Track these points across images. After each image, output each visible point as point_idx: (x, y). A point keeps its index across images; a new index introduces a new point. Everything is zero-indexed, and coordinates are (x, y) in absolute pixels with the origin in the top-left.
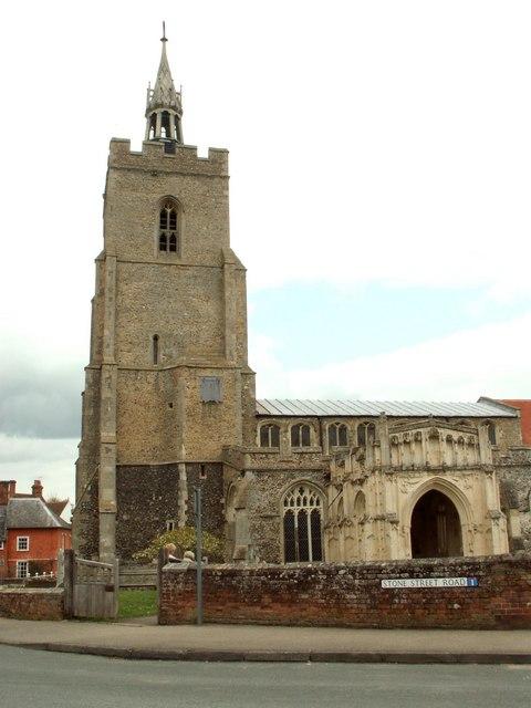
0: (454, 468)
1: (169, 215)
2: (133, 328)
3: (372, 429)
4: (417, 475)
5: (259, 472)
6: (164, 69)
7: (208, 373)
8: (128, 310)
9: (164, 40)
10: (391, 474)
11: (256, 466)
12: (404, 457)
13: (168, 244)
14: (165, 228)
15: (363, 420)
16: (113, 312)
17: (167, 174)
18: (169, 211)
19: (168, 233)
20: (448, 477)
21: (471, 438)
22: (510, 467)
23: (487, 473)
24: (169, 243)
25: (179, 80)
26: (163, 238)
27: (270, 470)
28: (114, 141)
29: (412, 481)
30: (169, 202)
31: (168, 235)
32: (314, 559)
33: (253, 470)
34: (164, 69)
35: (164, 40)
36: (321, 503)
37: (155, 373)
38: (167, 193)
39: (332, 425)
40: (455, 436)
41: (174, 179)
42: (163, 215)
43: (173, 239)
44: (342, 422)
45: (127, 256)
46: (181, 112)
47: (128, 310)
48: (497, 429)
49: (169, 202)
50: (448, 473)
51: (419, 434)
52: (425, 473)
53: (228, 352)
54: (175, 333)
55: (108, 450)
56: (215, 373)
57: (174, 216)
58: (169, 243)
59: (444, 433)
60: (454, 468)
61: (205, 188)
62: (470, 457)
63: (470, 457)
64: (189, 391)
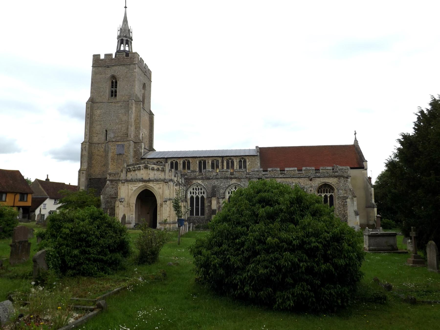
0: (152, 181)
1: (114, 83)
4: (137, 183)
6: (125, 20)
7: (120, 143)
8: (96, 121)
9: (126, 7)
10: (124, 183)
12: (130, 176)
13: (114, 94)
14: (112, 88)
15: (184, 159)
16: (89, 123)
17: (113, 66)
18: (114, 81)
19: (114, 89)
20: (151, 184)
21: (162, 168)
22: (217, 179)
23: (165, 182)
24: (114, 94)
25: (130, 24)
26: (112, 92)
27: (115, 180)
28: (94, 56)
29: (135, 185)
30: (113, 77)
32: (196, 215)
33: (109, 180)
34: (125, 20)
35: (126, 7)
37: (105, 144)
40: (155, 167)
42: (112, 82)
44: (176, 160)
45: (97, 101)
46: (132, 40)
47: (96, 121)
48: (247, 161)
49: (113, 77)
50: (151, 182)
51: (140, 167)
52: (141, 183)
54: (113, 128)
55: (83, 173)
56: (122, 143)
57: (116, 82)
58: (114, 94)
60: (152, 181)
61: (127, 70)
62: (161, 176)
63: (161, 176)
64: (112, 151)
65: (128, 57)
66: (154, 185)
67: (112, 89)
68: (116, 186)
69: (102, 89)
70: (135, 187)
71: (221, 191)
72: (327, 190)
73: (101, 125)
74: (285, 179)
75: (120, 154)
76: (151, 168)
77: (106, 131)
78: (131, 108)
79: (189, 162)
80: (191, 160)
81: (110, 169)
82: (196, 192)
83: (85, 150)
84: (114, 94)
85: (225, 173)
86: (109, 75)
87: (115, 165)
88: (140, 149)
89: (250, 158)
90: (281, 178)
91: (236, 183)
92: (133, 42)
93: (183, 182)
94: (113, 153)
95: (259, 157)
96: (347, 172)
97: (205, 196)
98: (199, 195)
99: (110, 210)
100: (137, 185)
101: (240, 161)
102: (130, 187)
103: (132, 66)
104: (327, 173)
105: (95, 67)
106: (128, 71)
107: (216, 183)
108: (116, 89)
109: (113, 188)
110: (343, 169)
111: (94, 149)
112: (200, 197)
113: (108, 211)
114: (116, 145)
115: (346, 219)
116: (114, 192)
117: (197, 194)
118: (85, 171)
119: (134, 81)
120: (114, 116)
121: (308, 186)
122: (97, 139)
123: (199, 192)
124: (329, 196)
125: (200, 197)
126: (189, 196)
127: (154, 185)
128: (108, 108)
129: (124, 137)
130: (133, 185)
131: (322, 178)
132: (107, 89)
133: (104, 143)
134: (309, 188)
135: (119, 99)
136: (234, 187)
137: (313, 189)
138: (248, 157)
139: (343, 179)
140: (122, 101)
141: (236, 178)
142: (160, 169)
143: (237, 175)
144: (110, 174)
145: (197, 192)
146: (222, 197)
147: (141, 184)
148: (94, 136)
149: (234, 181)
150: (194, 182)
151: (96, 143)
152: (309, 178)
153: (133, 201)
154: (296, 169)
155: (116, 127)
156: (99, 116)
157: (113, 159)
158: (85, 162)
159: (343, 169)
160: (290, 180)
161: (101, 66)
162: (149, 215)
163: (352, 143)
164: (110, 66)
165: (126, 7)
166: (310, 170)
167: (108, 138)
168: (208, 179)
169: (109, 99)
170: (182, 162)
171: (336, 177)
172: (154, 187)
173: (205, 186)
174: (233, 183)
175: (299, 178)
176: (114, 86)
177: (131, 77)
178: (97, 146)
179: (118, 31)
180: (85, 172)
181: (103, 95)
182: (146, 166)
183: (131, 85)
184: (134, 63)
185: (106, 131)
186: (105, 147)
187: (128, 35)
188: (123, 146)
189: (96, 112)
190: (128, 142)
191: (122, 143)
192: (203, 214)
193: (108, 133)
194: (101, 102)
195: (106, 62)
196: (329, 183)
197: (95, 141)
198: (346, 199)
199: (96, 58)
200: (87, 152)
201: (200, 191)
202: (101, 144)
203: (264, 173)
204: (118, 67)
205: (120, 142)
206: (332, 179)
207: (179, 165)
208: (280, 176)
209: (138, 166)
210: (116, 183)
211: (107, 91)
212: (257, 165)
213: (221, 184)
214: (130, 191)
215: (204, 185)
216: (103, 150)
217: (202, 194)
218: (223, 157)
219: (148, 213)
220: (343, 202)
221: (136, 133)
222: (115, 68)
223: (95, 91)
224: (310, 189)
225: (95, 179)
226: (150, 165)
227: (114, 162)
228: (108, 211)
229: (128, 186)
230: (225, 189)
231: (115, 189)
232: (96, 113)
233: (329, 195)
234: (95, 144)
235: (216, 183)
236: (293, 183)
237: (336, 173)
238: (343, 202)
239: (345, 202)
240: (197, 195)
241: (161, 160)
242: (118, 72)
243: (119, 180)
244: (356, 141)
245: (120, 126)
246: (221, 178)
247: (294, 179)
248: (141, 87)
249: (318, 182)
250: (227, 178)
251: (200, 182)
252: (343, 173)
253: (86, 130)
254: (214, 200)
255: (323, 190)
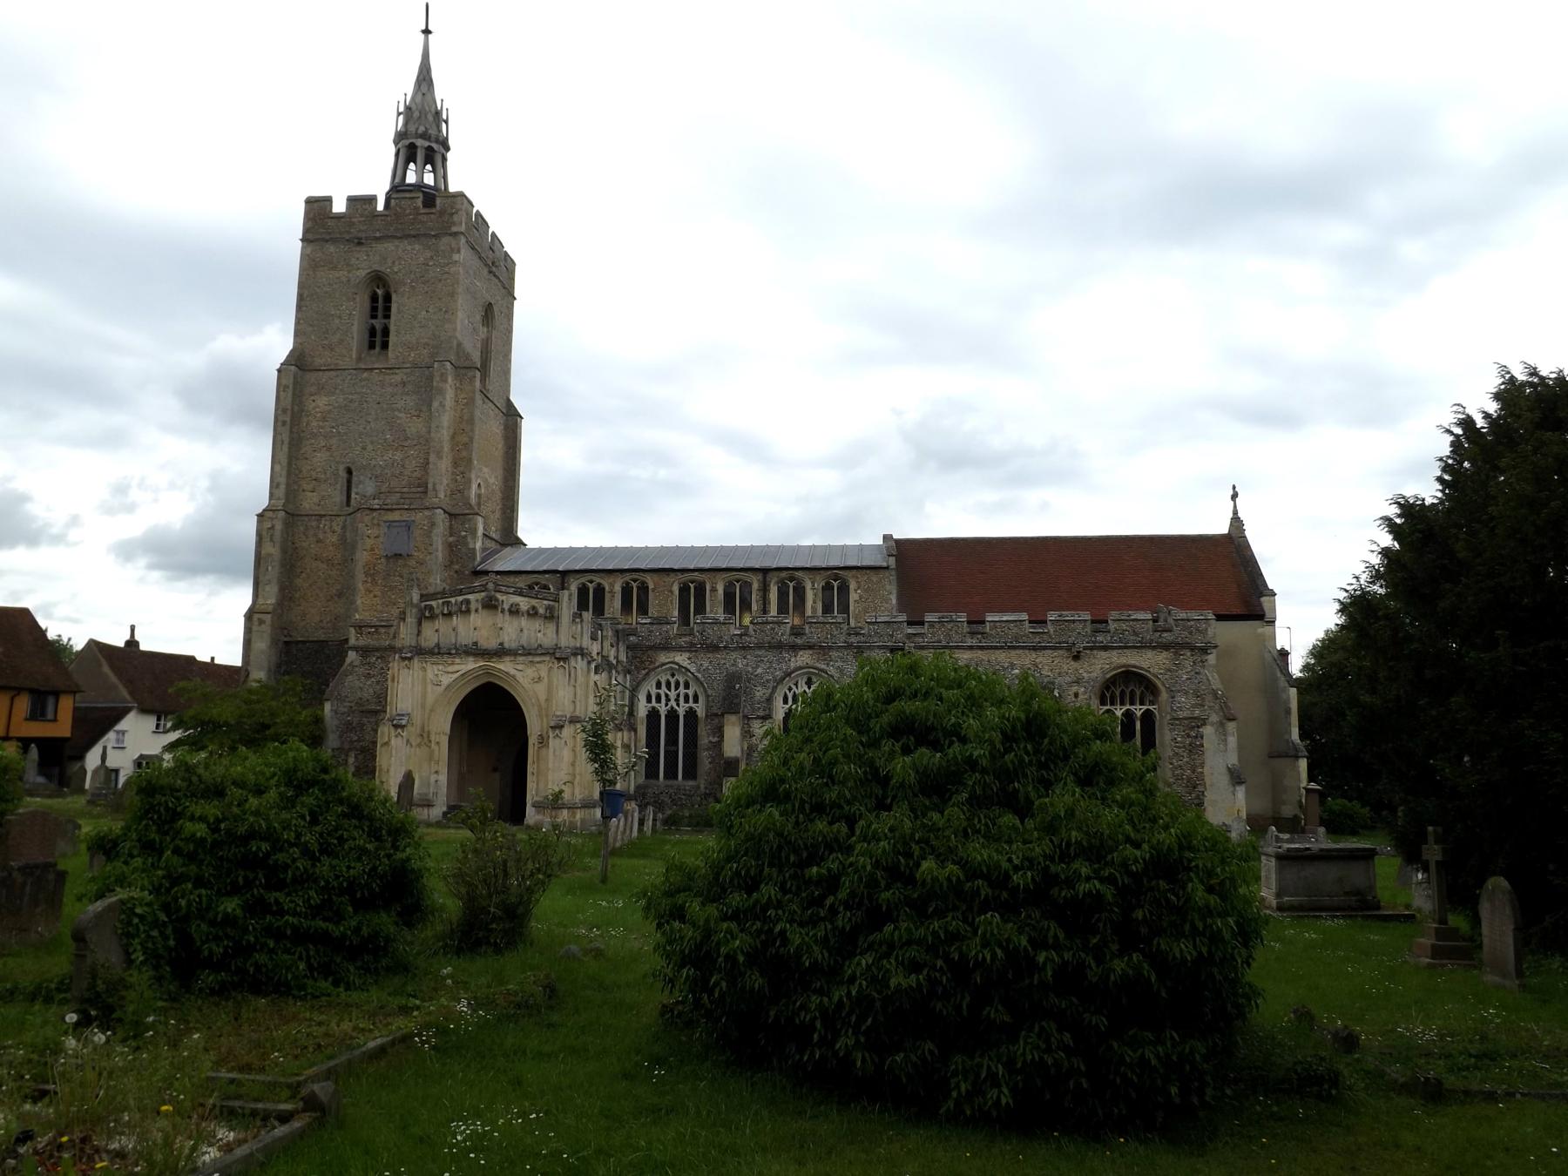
1: (380, 302)
2: (320, 458)
3: (844, 589)
4: (457, 660)
5: (365, 651)
6: (425, 78)
7: (396, 516)
9: (427, 32)
11: (361, 643)
13: (378, 339)
14: (374, 317)
15: (628, 577)
17: (377, 239)
18: (380, 292)
19: (378, 324)
20: (505, 666)
21: (549, 608)
22: (744, 648)
24: (378, 339)
25: (443, 92)
26: (372, 332)
27: (377, 650)
28: (311, 202)
29: (450, 669)
30: (378, 279)
31: (378, 327)
32: (666, 777)
34: (425, 78)
35: (427, 32)
36: (701, 699)
38: (376, 267)
39: (584, 585)
40: (524, 603)
41: (389, 246)
42: (374, 298)
43: (386, 332)
44: (597, 579)
45: (318, 362)
46: (448, 149)
48: (853, 586)
49: (378, 279)
50: (507, 659)
52: (471, 659)
53: (430, 486)
54: (373, 462)
56: (406, 516)
57: (388, 298)
58: (378, 339)
59: (508, 600)
61: (428, 254)
62: (542, 634)
63: (542, 634)
64: (369, 542)
65: (434, 211)
66: (520, 667)
67: (374, 321)
68: (382, 669)
69: (337, 321)
70: (450, 675)
71: (758, 694)
72: (1132, 693)
73: (329, 449)
74: (986, 652)
75: (396, 555)
76: (506, 607)
77: (349, 472)
78: (441, 392)
79: (644, 589)
80: (650, 581)
81: (360, 610)
82: (667, 695)
83: (271, 540)
84: (378, 339)
85: (773, 629)
86: (362, 273)
87: (379, 593)
88: (469, 539)
89: (863, 577)
90: (971, 648)
91: (810, 663)
92: (449, 155)
93: (623, 657)
94: (372, 550)
95: (893, 573)
96: (1204, 632)
97: (700, 709)
98: (678, 705)
99: (356, 757)
100: (456, 668)
101: (828, 588)
102: (430, 675)
103: (445, 240)
104: (1136, 634)
105: (312, 242)
106: (432, 258)
107: (740, 662)
108: (386, 321)
109: (368, 676)
110: (1188, 620)
111: (304, 534)
112: (681, 711)
113: (351, 760)
114: (382, 523)
115: (1198, 797)
116: (371, 691)
117: (673, 703)
118: (269, 616)
119: (452, 295)
120: (377, 419)
121: (1068, 679)
122: (316, 500)
123: (678, 695)
124: (1139, 714)
125: (681, 711)
126: (642, 709)
127: (520, 667)
128: (358, 390)
129: (411, 495)
130: (440, 667)
131: (1115, 652)
132: (356, 323)
133: (339, 513)
134: (1070, 684)
135: (398, 357)
136: (805, 680)
137: (1083, 689)
138: (854, 572)
139: (1189, 654)
140: (408, 365)
141: (810, 647)
142: (541, 611)
143: (813, 635)
144: (360, 627)
145: (673, 694)
146: (761, 713)
147: (471, 664)
148: (304, 491)
149: (804, 658)
150: (663, 658)
151: (311, 513)
152: (1069, 649)
153: (442, 723)
154: (1024, 616)
155: (385, 458)
156: (324, 419)
157: (370, 572)
158: (269, 582)
159: (1188, 620)
160: (1002, 657)
161: (334, 241)
162: (497, 776)
163: (1221, 527)
164: (367, 238)
165: (430, 32)
166: (1074, 621)
167: (353, 496)
168: (714, 648)
169: (359, 359)
170: (618, 588)
171: (1166, 647)
172: (519, 675)
173: (699, 676)
174: (799, 664)
175: (1034, 649)
176: (380, 313)
177: (440, 280)
178: (314, 524)
179: (399, 114)
180: (268, 618)
181: (341, 341)
182: (491, 598)
183: (441, 310)
184: (454, 229)
185: (349, 472)
186: (344, 527)
187: (433, 132)
188: (408, 526)
189: (314, 404)
190: (427, 513)
191: (406, 516)
192: (691, 773)
193: (355, 479)
194: (332, 367)
195: (354, 223)
196: (1142, 669)
197: (307, 506)
198: (1198, 727)
199: (317, 208)
200: (278, 545)
201: (682, 690)
202: (328, 518)
203: (910, 631)
204: (397, 242)
205: (397, 512)
206: (1150, 654)
207: (607, 596)
208: (974, 642)
209: (460, 598)
210: (381, 657)
211: (355, 328)
212: (888, 601)
213: (758, 667)
214: (429, 687)
215: (699, 671)
216: (334, 539)
217: (691, 704)
218: (765, 571)
219: (495, 770)
220: (1189, 736)
221: (456, 481)
222: (381, 247)
223: (311, 329)
224: (1075, 689)
225: (304, 642)
226: (504, 598)
227: (374, 582)
228: (351, 760)
229: (424, 669)
230: (771, 684)
231: (378, 682)
232: (314, 408)
233: (1139, 710)
234: (306, 519)
235: (740, 662)
236: (1012, 669)
237: (1165, 635)
238: (1189, 736)
239: (1196, 737)
240: (672, 708)
241: (543, 579)
242: (394, 262)
243: (392, 649)
244: (1236, 521)
245: (398, 456)
246: (760, 648)
247: (1018, 652)
248: (478, 318)
249: (1100, 665)
250: (779, 647)
251: (682, 659)
252: (1191, 633)
253: (278, 468)
254: (733, 724)
255: (1118, 693)
